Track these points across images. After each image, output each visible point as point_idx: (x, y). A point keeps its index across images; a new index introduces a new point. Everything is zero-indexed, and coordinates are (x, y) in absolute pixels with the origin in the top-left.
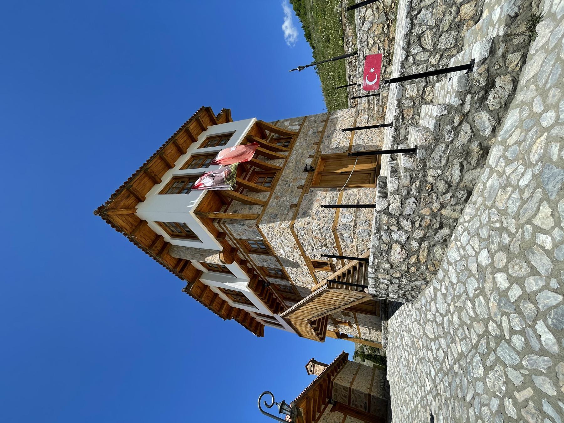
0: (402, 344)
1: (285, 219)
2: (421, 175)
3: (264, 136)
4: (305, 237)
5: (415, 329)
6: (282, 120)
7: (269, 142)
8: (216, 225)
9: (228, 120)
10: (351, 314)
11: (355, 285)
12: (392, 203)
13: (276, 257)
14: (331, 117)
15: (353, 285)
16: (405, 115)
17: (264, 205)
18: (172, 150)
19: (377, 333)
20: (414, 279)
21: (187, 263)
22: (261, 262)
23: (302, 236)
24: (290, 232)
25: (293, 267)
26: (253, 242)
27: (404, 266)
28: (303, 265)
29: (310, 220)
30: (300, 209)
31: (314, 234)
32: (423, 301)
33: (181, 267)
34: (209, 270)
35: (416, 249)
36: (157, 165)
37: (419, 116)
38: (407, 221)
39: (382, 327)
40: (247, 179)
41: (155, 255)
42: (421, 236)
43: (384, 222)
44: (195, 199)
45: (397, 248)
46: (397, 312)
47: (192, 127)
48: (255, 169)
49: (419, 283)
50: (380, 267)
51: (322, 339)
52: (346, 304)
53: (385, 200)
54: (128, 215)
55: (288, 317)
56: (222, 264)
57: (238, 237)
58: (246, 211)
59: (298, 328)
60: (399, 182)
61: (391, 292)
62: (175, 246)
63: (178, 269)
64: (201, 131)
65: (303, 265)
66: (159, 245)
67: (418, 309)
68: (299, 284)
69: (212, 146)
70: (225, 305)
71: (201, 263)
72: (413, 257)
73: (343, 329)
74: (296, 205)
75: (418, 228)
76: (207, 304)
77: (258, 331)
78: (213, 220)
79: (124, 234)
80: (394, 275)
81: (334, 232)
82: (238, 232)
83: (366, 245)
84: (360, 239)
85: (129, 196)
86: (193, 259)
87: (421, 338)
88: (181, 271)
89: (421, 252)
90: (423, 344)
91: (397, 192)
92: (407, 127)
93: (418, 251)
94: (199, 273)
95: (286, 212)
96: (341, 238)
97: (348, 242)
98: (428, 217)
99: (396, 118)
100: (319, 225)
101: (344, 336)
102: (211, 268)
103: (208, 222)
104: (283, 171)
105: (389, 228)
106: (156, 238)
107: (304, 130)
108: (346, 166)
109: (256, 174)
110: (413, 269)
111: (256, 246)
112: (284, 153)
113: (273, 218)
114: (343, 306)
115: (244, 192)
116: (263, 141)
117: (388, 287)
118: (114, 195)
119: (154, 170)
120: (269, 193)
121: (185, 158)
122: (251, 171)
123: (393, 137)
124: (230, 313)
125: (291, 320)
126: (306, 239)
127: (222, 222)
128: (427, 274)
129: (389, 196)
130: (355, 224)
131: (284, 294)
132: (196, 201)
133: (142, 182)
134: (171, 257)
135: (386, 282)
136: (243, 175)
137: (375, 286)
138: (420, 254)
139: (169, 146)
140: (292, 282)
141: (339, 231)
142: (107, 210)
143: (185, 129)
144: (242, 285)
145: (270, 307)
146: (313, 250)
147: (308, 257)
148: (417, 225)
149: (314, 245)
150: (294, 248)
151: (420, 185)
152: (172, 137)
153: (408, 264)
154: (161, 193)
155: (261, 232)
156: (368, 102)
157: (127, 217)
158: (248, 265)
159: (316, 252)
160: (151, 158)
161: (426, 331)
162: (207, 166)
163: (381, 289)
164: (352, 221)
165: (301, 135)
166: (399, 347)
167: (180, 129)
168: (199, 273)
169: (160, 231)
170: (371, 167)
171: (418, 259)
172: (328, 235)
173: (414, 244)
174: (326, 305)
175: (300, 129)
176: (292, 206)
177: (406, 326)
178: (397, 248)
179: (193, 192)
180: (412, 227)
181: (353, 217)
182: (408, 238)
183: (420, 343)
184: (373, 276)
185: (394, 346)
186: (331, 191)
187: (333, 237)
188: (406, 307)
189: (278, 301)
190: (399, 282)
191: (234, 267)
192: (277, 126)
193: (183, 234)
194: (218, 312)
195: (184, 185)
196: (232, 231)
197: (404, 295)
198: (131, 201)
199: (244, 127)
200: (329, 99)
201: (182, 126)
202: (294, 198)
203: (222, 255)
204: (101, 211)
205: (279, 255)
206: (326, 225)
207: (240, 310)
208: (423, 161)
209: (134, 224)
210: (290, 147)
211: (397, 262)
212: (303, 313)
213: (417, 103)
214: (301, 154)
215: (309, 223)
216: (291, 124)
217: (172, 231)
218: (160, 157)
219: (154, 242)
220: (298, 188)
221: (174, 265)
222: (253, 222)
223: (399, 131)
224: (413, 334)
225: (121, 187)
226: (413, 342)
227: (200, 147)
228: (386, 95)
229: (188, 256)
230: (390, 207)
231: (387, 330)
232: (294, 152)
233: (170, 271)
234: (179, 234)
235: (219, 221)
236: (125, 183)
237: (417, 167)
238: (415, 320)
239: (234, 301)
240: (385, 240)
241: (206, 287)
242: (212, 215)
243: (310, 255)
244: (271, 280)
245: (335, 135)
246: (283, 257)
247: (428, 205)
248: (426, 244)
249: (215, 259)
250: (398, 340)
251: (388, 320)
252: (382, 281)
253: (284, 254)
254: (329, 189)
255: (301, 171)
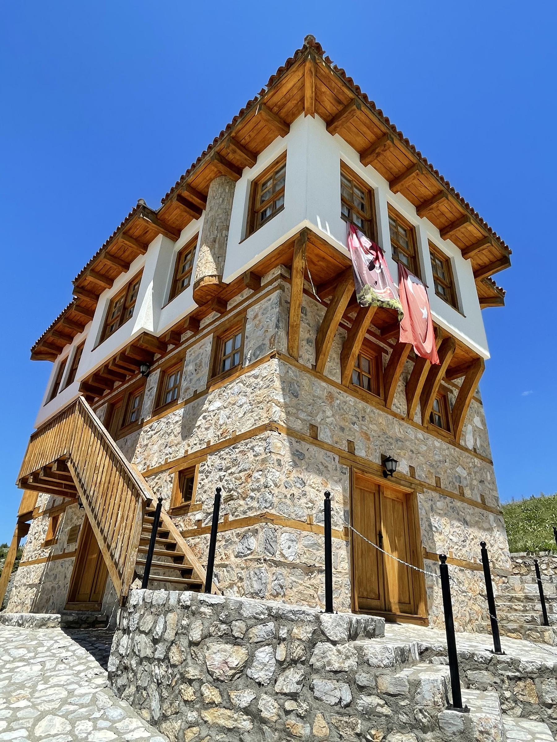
0: (14, 660)
1: (288, 413)
2: (404, 718)
3: (451, 373)
4: (251, 454)
5: (50, 691)
6: (482, 410)
7: (441, 385)
8: (277, 271)
9: (483, 300)
10: (74, 547)
11: (149, 559)
12: (338, 651)
13: (205, 392)
14: (491, 517)
15: (150, 554)
16: (521, 684)
17: (316, 370)
18: (426, 186)
19: (28, 602)
20: (165, 694)
21: (197, 211)
22: (195, 359)
23: (252, 448)
24: (261, 423)
25: (183, 426)
26: (238, 345)
27: (197, 672)
28: (186, 448)
29: (287, 467)
30: (308, 446)
31: (256, 475)
32: (115, 713)
33: (192, 200)
34: (180, 253)
35: (235, 701)
36: (397, 158)
37: (522, 716)
38: (298, 683)
39: (47, 616)
40: (368, 336)
41: (217, 149)
42: (265, 714)
43: (295, 631)
44: (331, 230)
45: (237, 656)
46: (82, 651)
47: (472, 229)
48: (387, 353)
49: (155, 704)
50: (192, 618)
51: (24, 483)
52: (105, 539)
53: (345, 636)
54: (302, 100)
55: (77, 413)
56: (193, 281)
57: (250, 314)
58: (305, 333)
59: (51, 433)
60: (386, 666)
61: (133, 639)
62: (232, 187)
63: (186, 194)
64: (462, 245)
65: (186, 448)
66: (236, 156)
67: (94, 700)
68: (143, 437)
69: (434, 267)
70: (102, 284)
71: (196, 238)
72: (216, 692)
73: (39, 527)
74: (315, 438)
75: (282, 707)
76: (109, 248)
77: (43, 349)
78: (289, 266)
79: (263, 90)
80: (174, 649)
81: (263, 517)
82: (262, 315)
83: (231, 586)
84: (244, 574)
85: (339, 102)
86: (206, 222)
87: (34, 706)
88: (181, 199)
89: (228, 712)
90: (19, 709)
91: (364, 662)
92: (496, 686)
93: (231, 706)
94: (174, 233)
95: (303, 416)
96: (246, 532)
97: (239, 548)
98: (308, 730)
99: (514, 663)
100: (276, 485)
101: (23, 529)
102: (185, 257)
103: (285, 257)
104: (383, 411)
105: (281, 640)
106: (251, 152)
107: (466, 458)
108: (394, 548)
109: (378, 356)
110: (189, 693)
111: (229, 350)
112: (419, 415)
113: (290, 389)
114: (102, 531)
115: (342, 330)
116: (442, 373)
117: (146, 634)
118: (343, 73)
119: (388, 153)
120: (339, 381)
121: (408, 212)
122: (382, 345)
123: (473, 655)
124: (86, 292)
125: (71, 418)
126: (247, 456)
127: (283, 283)
128: (177, 725)
129: (353, 643)
130: (278, 564)
131: (121, 405)
132: (329, 233)
133: (365, 129)
134: (211, 180)
135: (159, 629)
136: (374, 329)
137: (148, 605)
138: (223, 711)
139: (433, 181)
140: (148, 422)
141: (262, 528)
142: (314, 59)
143: (466, 215)
144: (146, 319)
145: (96, 375)
146: (220, 470)
147: (206, 460)
148: (289, 705)
149: (232, 473)
150: (226, 431)
151: (380, 715)
152: (453, 190)
153: (201, 682)
154: (343, 165)
155: (261, 361)
156: (528, 598)
157: (298, 97)
158: (189, 333)
159: (215, 475)
160: (413, 147)
161: (49, 717)
162: (395, 257)
163: (142, 616)
164: (283, 555)
165: (455, 452)
166: (6, 651)
167: (467, 205)
168: (174, 233)
169: (265, 160)
170: (392, 600)
171: (212, 704)
172: (255, 504)
173: (245, 698)
174: (105, 494)
175: (466, 449)
176: (314, 428)
177: (54, 669)
178: (237, 656)
179: (343, 225)
180: (285, 694)
181: (291, 558)
182: (259, 684)
183: (23, 703)
184: (173, 601)
185: (8, 641)
186: (345, 511)
187: (251, 514)
188: (96, 671)
189: (107, 391)
190: (159, 660)
191: (185, 304)
192: (473, 400)
193: (258, 205)
194: (90, 268)
195: (359, 210)
196: (264, 303)
197: (126, 668)
198: (328, 108)
199: (471, 333)
200: (518, 510)
201: (472, 210)
202: (329, 434)
203: (215, 281)
204: (313, 49)
205: (210, 397)
206: (275, 500)
207: (90, 313)
208: (435, 725)
209: (284, 110)
210: (431, 426)
211: (205, 657)
212: (83, 443)
213: (550, 711)
214: (417, 450)
215: (280, 465)
216: (475, 430)
217: (264, 184)
218: (414, 165)
219: (244, 148)
220: (350, 442)
221: (193, 184)
222: (283, 348)
223: (487, 669)
224: (40, 687)
225: (358, 88)
226: (22, 686)
227: (431, 244)
228: (546, 639)
229: (212, 213)
230: (329, 645)
231: (40, 627)
232: (420, 436)
233: (182, 178)
234: (258, 197)
235: (287, 278)
236: (365, 97)
237: (421, 711)
238: (71, 693)
239: (112, 301)
240: (255, 630)
241: (144, 247)
242: (299, 263)
243: (209, 463)
244: (154, 379)
245: (457, 524)
246: (205, 407)
247: (334, 733)
248: (246, 724)
249: (204, 267)
250: (22, 652)
251: (63, 628)
252: (161, 620)
253: (211, 408)
254: (348, 508)
255: (382, 448)
